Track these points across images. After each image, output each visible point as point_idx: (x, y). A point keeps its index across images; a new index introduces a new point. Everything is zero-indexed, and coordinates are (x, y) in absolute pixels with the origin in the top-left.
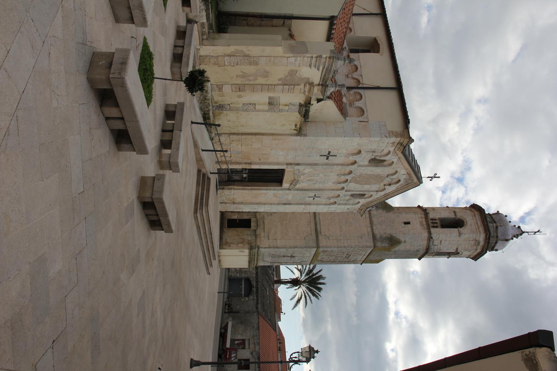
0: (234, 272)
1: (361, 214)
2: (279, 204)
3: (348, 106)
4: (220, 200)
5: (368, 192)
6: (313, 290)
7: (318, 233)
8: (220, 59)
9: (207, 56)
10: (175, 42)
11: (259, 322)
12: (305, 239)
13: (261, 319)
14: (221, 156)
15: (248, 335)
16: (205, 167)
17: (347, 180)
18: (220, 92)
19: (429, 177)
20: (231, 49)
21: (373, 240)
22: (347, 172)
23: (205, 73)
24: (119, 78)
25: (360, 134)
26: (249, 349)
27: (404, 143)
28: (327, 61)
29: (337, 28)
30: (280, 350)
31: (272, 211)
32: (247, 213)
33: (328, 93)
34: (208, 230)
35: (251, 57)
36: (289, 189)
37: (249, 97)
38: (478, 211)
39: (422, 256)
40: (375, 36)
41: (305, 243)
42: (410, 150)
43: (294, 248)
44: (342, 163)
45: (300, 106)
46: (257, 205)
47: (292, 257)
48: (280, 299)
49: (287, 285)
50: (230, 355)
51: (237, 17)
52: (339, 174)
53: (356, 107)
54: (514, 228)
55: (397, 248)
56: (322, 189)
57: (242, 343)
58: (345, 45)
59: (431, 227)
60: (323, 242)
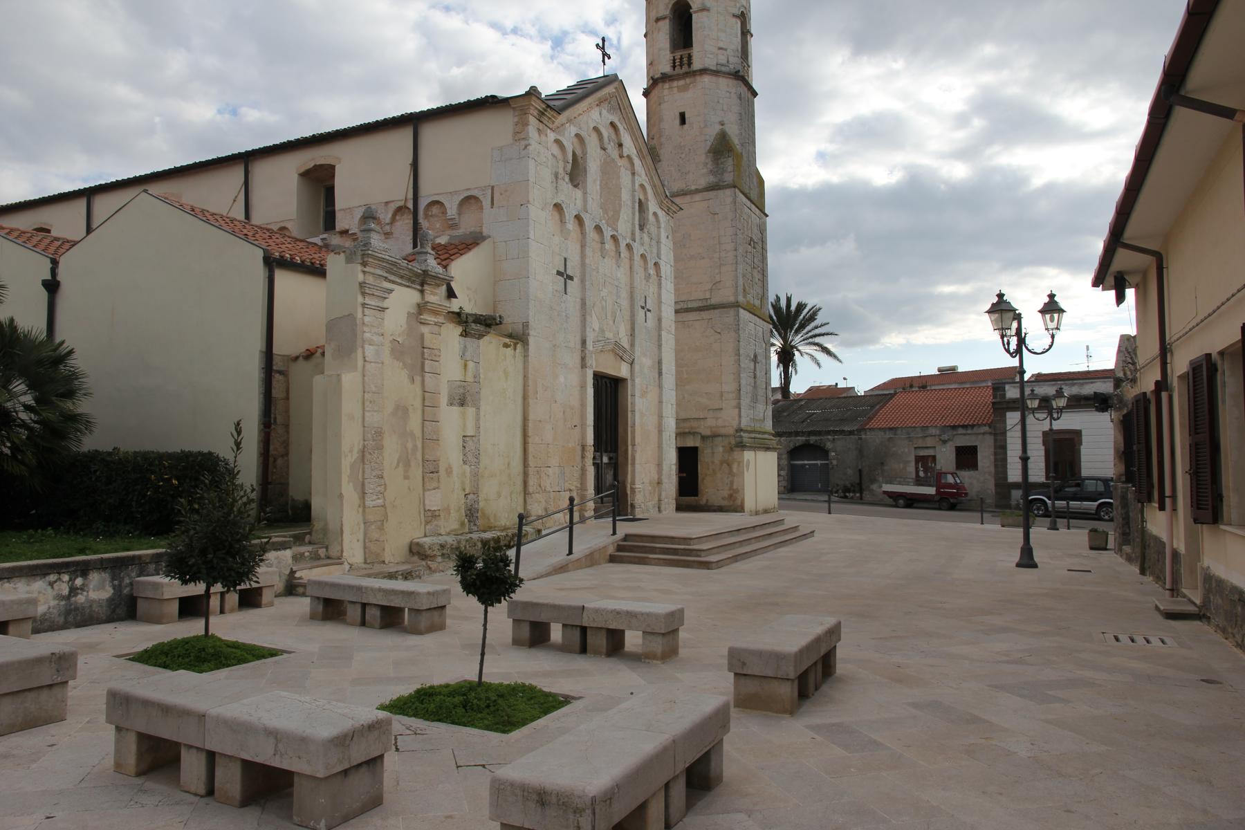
1: (678, 209)
2: (660, 386)
3: (458, 231)
4: (653, 513)
6: (802, 321)
7: (706, 304)
8: (371, 518)
9: (365, 548)
10: (352, 624)
11: (880, 429)
12: (719, 333)
13: (873, 424)
17: (613, 237)
18: (439, 516)
19: (604, 61)
20: (349, 491)
21: (720, 189)
24: (594, 813)
25: (522, 205)
26: (935, 447)
28: (372, 270)
29: (290, 252)
30: (924, 387)
34: (733, 536)
35: (364, 447)
36: (632, 364)
40: (296, 176)
41: (729, 332)
42: (552, 98)
44: (578, 247)
45: (466, 336)
46: (664, 433)
47: (755, 359)
48: (810, 390)
50: (950, 486)
51: (270, 480)
52: (602, 252)
53: (459, 214)
55: (736, 141)
56: (631, 292)
57: (925, 462)
58: (317, 240)
59: (691, 69)
60: (726, 295)
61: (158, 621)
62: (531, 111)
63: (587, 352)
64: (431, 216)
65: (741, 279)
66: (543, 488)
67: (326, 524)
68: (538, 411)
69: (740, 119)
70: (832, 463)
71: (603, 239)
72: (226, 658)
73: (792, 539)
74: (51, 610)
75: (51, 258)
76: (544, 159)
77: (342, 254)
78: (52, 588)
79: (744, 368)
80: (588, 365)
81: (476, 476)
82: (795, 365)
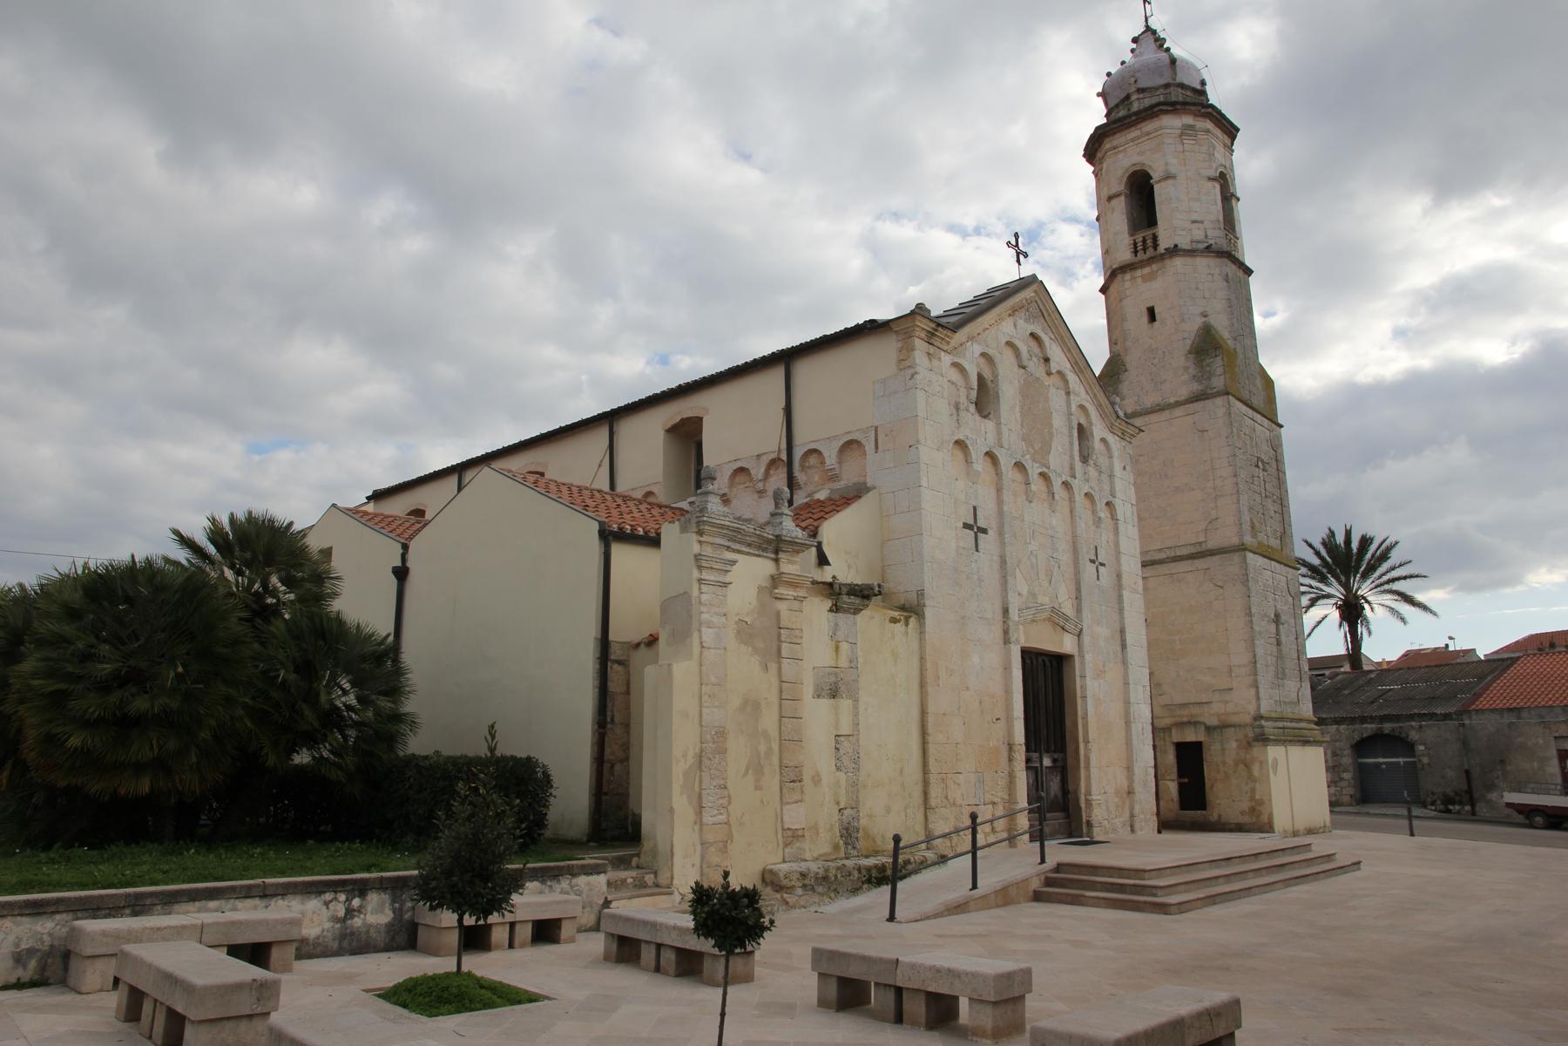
0: (1339, 789)
1: (1137, 431)
2: (1125, 662)
4: (1124, 833)
5: (1073, 417)
7: (1200, 550)
8: (710, 837)
10: (646, 970)
11: (1493, 711)
12: (1222, 587)
13: (1482, 703)
14: (993, 830)
15: (1541, 741)
16: (1026, 880)
17: (1042, 475)
18: (804, 836)
19: (1018, 261)
20: (681, 803)
21: (1208, 398)
22: (1018, 477)
23: (702, 886)
25: (910, 446)
27: (925, 327)
28: (710, 539)
31: (1146, 681)
32: (1158, 754)
33: (799, 534)
34: (1218, 867)
35: (702, 750)
36: (1079, 635)
37: (818, 755)
38: (1103, 142)
39: (1239, 267)
40: (661, 434)
42: (948, 313)
43: (1250, 614)
44: (993, 491)
46: (1133, 725)
47: (1277, 619)
49: (1362, 634)
51: (605, 790)
53: (840, 462)
54: (1137, 52)
56: (1074, 543)
59: (1158, 252)
60: (1226, 535)
61: (433, 952)
62: (917, 334)
63: (1010, 624)
64: (808, 467)
65: (1246, 513)
66: (952, 801)
67: (655, 845)
68: (939, 702)
69: (1229, 307)
70: (1420, 761)
71: (1028, 478)
72: (471, 1001)
73: (1317, 873)
74: (325, 933)
75: (402, 543)
76: (939, 389)
77: (677, 523)
78: (328, 908)
79: (1260, 633)
80: (1013, 639)
81: (854, 786)
82: (1366, 622)
